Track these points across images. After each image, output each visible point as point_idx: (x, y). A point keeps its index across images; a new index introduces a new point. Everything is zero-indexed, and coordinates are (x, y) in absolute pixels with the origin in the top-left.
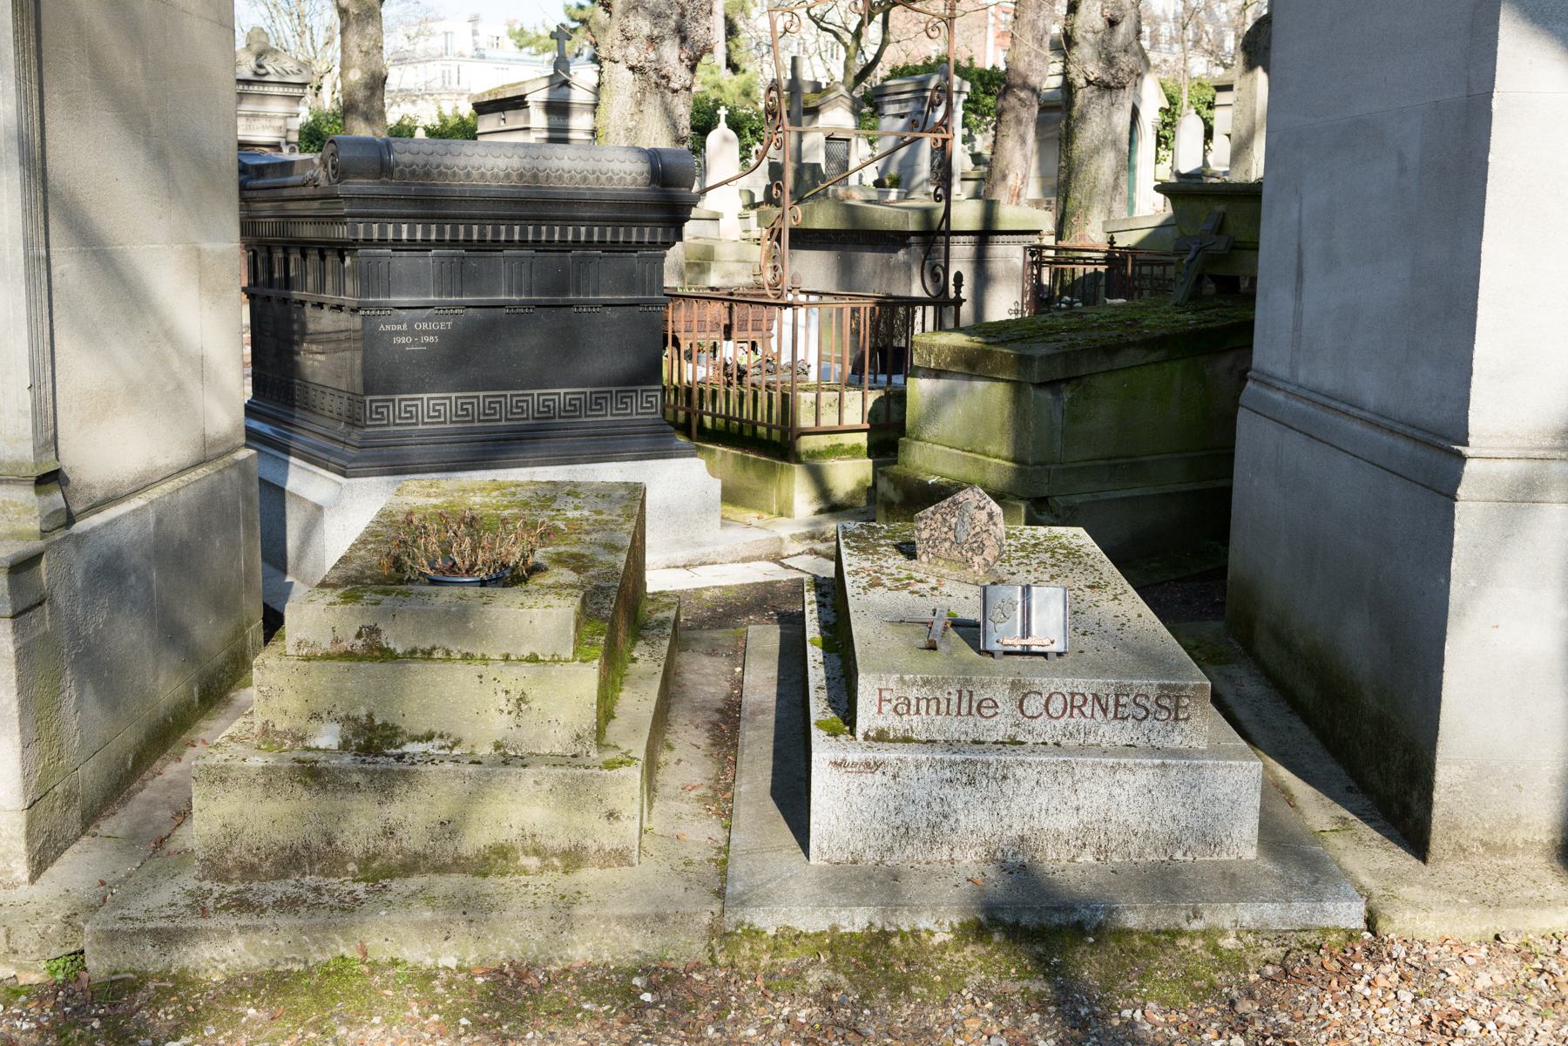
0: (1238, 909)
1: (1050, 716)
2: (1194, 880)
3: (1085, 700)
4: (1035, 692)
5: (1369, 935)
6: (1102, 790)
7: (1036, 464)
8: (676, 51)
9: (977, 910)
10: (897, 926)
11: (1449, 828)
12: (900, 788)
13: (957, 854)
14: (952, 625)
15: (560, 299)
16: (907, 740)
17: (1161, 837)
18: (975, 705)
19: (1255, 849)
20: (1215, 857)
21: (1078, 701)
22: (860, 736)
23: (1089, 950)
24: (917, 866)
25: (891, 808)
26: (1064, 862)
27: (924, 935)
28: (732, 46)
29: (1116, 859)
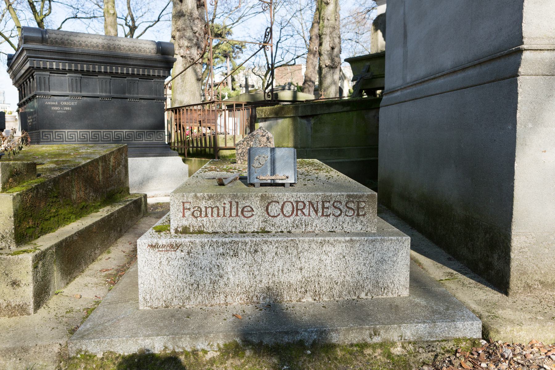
0: (402, 328)
1: (285, 216)
2: (373, 310)
3: (305, 205)
4: (275, 201)
5: (485, 342)
6: (315, 257)
7: (301, 148)
8: (196, 51)
9: (235, 335)
10: (183, 348)
11: (521, 274)
12: (192, 260)
13: (229, 299)
14: (240, 179)
15: (122, 96)
16: (200, 232)
17: (352, 284)
18: (240, 210)
19: (408, 290)
20: (385, 296)
21: (301, 206)
22: (173, 231)
23: (308, 359)
24: (204, 308)
25: (188, 272)
26: (294, 302)
27: (201, 354)
28: (233, 84)
29: (326, 299)
